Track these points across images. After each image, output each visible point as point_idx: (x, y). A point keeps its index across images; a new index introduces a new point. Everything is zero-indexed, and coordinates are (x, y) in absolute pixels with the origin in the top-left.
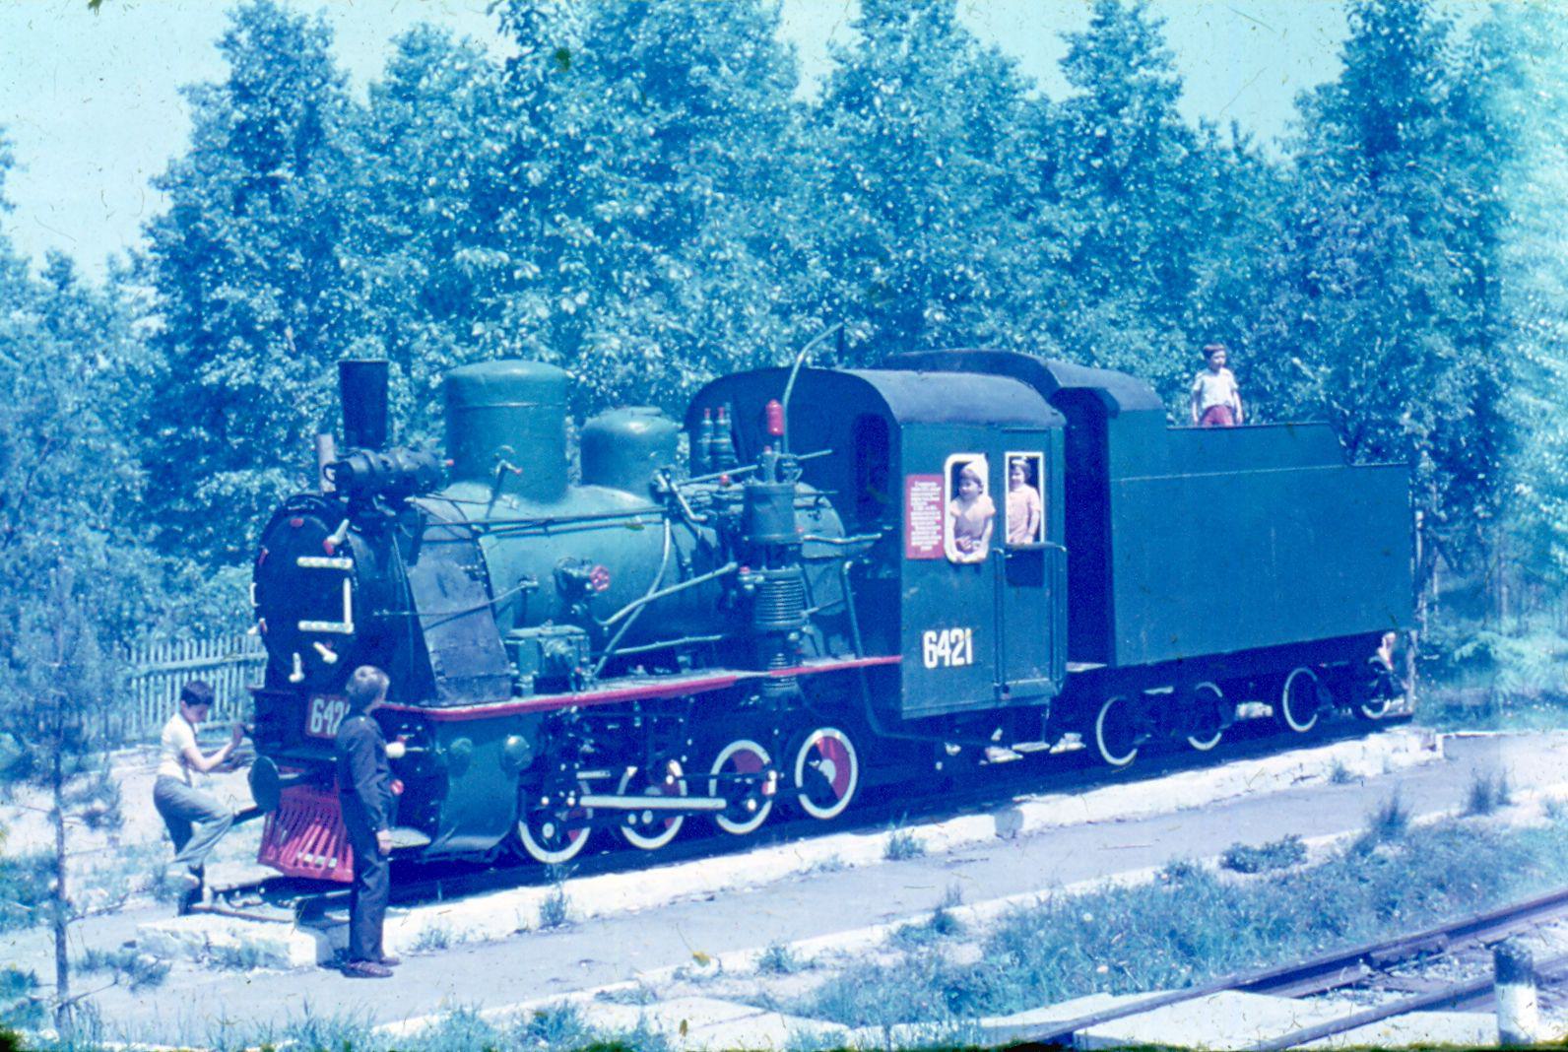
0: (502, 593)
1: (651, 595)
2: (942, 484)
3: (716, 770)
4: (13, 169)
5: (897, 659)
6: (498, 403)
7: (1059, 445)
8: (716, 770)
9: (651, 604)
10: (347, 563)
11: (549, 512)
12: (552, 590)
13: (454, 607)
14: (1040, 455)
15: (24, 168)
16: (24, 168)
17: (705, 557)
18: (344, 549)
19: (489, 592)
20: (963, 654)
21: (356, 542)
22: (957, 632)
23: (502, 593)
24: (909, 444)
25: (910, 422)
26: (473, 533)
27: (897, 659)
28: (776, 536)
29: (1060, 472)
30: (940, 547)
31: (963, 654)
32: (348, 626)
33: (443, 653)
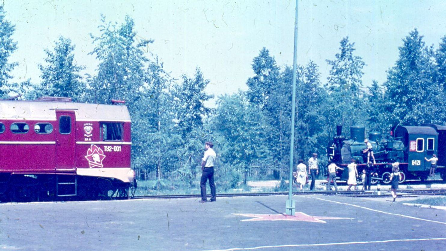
0: (352, 152)
1: (89, 161)
2: (416, 142)
3: (383, 175)
4: (364, 66)
5: (408, 163)
6: (356, 130)
7: (437, 138)
8: (383, 175)
9: (88, 161)
10: (334, 148)
11: (361, 143)
12: (360, 152)
13: (346, 153)
14: (434, 139)
15: (367, 65)
16: (367, 65)
17: (382, 149)
18: (334, 146)
19: (351, 152)
20: (419, 163)
21: (335, 146)
22: (418, 161)
23: (352, 152)
24: (410, 136)
25: (411, 134)
26: (349, 145)
27: (408, 163)
28: (390, 147)
29: (437, 141)
30: (415, 150)
31: (419, 163)
32: (333, 155)
33: (344, 158)
